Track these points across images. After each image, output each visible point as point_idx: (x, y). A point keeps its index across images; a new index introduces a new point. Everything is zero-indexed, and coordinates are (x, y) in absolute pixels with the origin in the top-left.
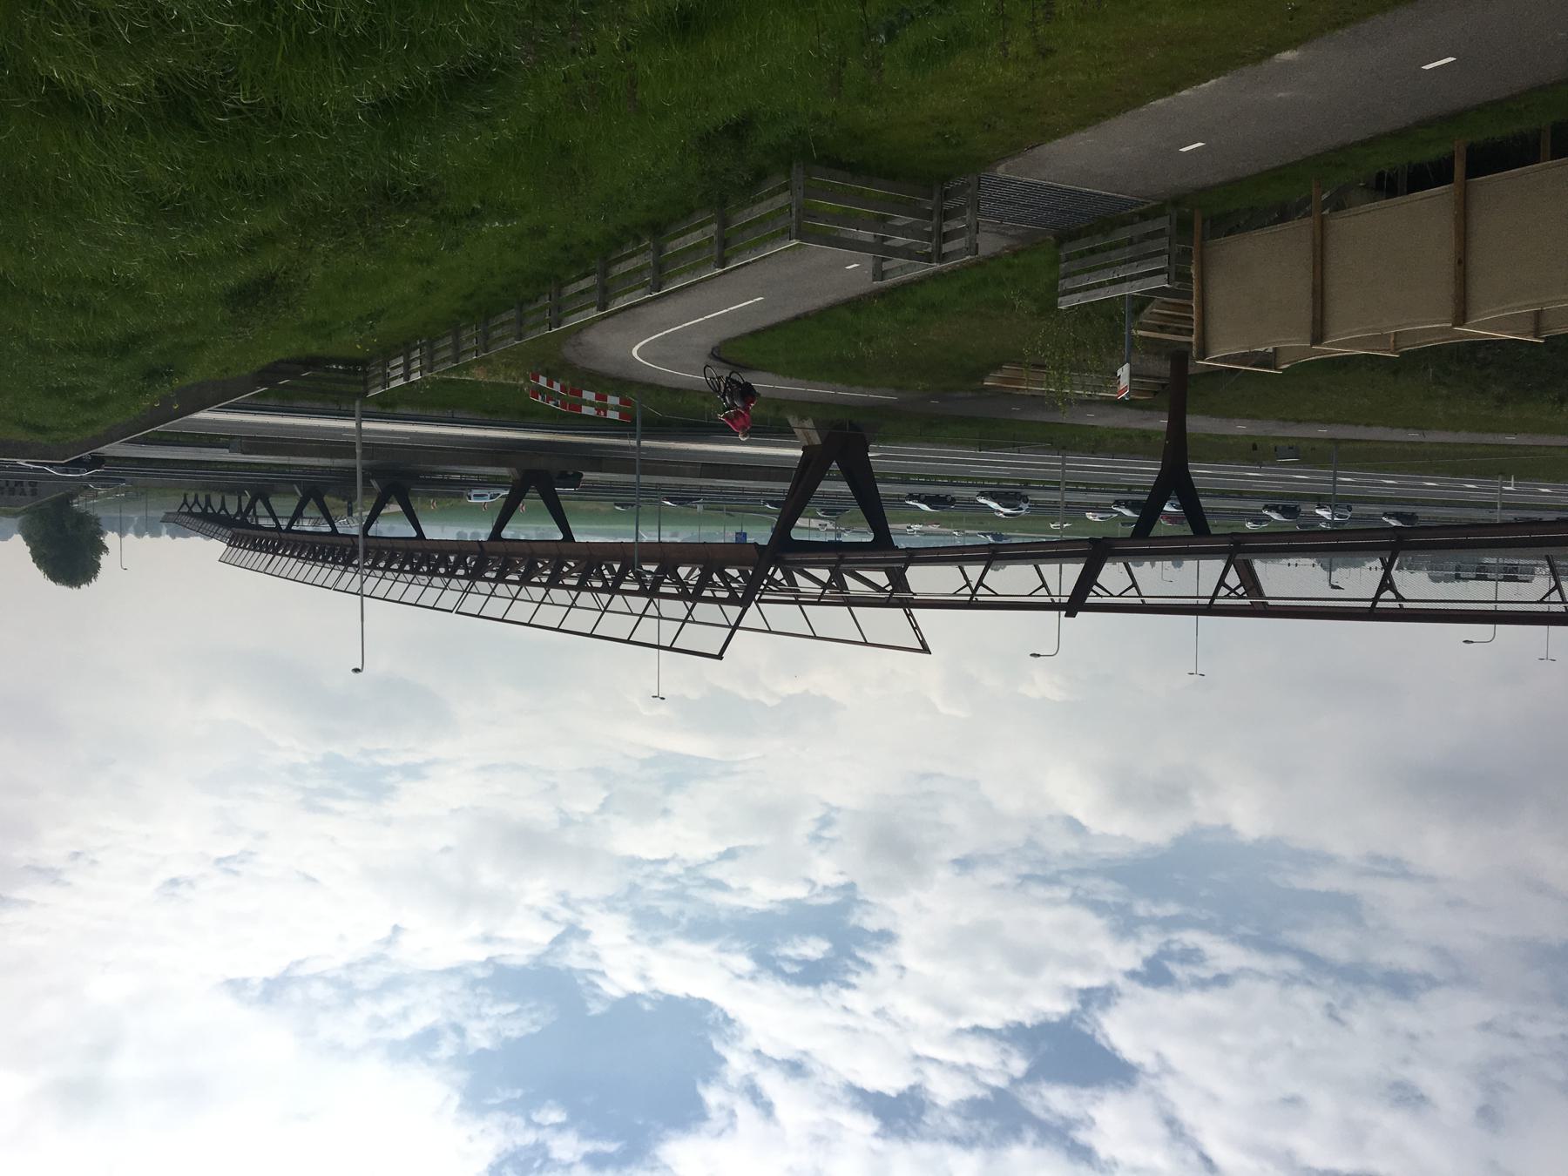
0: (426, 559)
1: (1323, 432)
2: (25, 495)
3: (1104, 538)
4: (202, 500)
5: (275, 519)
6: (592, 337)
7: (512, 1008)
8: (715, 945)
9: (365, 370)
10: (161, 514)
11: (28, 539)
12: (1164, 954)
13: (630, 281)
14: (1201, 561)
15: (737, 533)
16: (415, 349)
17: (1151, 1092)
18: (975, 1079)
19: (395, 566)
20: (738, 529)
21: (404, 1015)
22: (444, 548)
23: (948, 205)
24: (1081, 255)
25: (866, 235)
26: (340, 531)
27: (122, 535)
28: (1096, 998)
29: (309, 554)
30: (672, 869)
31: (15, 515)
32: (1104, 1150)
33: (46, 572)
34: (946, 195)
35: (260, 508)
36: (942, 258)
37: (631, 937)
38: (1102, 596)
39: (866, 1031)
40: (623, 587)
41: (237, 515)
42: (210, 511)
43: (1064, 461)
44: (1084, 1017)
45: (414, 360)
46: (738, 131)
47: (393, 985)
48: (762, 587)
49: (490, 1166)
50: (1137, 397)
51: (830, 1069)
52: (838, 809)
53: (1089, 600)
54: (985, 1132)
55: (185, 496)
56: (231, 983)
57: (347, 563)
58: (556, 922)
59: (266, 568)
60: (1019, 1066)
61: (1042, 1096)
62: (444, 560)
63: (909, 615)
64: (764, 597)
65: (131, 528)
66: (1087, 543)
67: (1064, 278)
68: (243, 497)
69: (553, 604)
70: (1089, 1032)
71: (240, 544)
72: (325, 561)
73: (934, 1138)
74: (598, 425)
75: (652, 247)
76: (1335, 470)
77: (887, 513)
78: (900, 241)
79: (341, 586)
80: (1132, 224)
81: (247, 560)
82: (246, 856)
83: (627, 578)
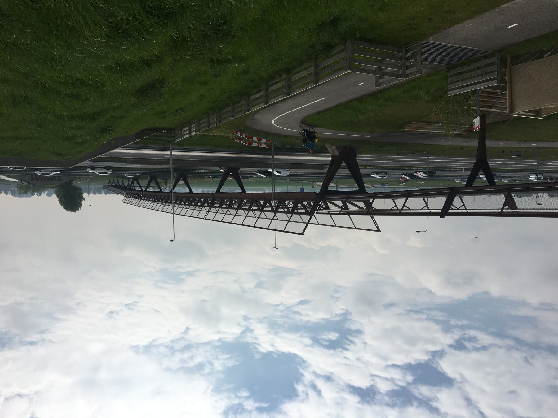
0: (194, 200)
1: (534, 145)
2: (56, 180)
3: (455, 187)
4: (116, 181)
5: (141, 187)
6: (258, 117)
7: (229, 356)
8: (299, 334)
9: (174, 132)
10: (102, 186)
11: (58, 196)
12: (463, 338)
13: (277, 92)
14: (475, 196)
15: (301, 189)
16: (193, 123)
17: (459, 388)
18: (394, 383)
19: (178, 202)
20: (301, 187)
21: (192, 358)
22: (200, 196)
23: (408, 55)
24: (456, 75)
25: (373, 67)
26: (163, 191)
27: (89, 194)
28: (438, 354)
29: (153, 199)
30: (281, 308)
31: (53, 188)
32: (443, 408)
33: (64, 207)
34: (407, 51)
35: (135, 183)
36: (406, 76)
37: (268, 332)
38: (454, 210)
39: (353, 365)
40: (265, 209)
41: (128, 186)
42: (118, 185)
43: (428, 159)
44: (433, 361)
45: (192, 128)
46: (334, 21)
47: (188, 347)
48: (318, 208)
49: (224, 411)
50: (463, 133)
51: (341, 379)
52: (340, 287)
53: (450, 211)
54: (398, 402)
55: (110, 180)
56: (132, 347)
57: (166, 202)
58: (242, 326)
59: (138, 205)
60: (410, 378)
61: (418, 389)
62: (200, 201)
63: (372, 218)
64: (318, 212)
65: (92, 191)
66: (448, 189)
67: (450, 84)
68: (130, 180)
69: (212, 212)
70: (435, 367)
71: (129, 196)
72: (158, 201)
73: (380, 404)
74: (260, 150)
75: (286, 78)
76: (538, 160)
77: (364, 180)
78: (389, 69)
79: (164, 210)
80: (480, 61)
81: (131, 202)
82: (135, 303)
83: (266, 206)
